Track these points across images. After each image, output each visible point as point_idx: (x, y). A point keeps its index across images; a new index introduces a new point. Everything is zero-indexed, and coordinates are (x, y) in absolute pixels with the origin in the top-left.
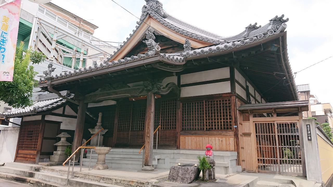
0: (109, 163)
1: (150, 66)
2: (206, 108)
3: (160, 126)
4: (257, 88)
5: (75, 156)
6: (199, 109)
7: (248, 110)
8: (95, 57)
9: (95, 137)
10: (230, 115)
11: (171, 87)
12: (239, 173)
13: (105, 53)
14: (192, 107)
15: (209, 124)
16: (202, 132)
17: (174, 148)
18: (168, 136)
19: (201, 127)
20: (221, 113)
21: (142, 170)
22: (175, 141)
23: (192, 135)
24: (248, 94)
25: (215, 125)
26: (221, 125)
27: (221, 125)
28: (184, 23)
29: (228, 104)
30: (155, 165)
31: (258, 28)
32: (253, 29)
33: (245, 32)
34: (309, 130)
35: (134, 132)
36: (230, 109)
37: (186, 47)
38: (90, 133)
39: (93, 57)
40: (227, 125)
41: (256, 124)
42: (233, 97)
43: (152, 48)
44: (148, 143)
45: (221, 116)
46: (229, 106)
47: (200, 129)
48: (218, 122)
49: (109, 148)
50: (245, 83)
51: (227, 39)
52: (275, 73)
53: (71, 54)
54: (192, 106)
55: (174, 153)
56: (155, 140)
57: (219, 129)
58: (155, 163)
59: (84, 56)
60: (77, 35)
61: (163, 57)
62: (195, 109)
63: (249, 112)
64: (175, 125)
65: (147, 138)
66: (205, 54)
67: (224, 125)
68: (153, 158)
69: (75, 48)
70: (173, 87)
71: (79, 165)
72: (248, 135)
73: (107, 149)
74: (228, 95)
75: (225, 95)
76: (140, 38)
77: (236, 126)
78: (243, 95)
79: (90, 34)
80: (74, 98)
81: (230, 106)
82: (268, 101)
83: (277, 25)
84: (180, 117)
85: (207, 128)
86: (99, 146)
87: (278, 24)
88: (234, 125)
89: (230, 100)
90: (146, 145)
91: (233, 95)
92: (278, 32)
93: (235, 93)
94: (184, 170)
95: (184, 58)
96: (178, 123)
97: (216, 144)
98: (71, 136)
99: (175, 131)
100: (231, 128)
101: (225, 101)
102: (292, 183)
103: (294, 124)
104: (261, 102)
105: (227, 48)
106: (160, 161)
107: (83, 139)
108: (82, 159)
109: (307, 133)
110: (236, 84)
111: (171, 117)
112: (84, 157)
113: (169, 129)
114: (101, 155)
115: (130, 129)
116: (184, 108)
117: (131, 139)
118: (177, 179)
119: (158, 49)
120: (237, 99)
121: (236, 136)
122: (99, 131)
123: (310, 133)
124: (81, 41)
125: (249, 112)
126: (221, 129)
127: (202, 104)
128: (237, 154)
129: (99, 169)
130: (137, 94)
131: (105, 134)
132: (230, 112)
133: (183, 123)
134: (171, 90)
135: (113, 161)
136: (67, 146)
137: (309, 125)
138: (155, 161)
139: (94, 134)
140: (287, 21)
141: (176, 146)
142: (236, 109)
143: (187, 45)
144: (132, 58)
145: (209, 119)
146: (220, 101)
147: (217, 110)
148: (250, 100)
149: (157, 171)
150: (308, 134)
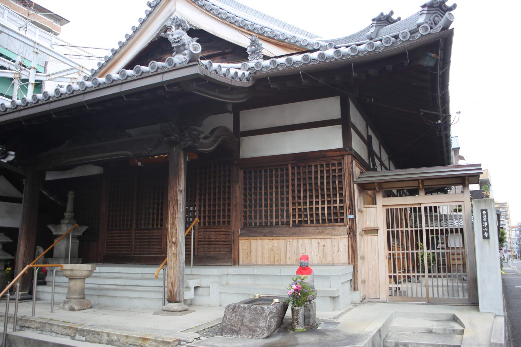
0: (94, 295)
1: (176, 88)
2: (293, 180)
3: (197, 219)
4: (383, 143)
5: (18, 284)
6: (279, 183)
7: (374, 183)
8: (60, 77)
9: (61, 241)
10: (341, 195)
11: (219, 137)
12: (356, 306)
13: (81, 69)
14: (263, 179)
15: (300, 213)
16: (284, 229)
17: (227, 262)
18: (213, 239)
19: (284, 218)
20: (323, 190)
21: (164, 311)
22: (229, 250)
23: (265, 236)
24: (371, 153)
25: (312, 215)
26: (323, 214)
27: (323, 214)
28: (245, 7)
29: (337, 171)
30: (190, 300)
31: (395, 21)
32: (386, 23)
33: (371, 27)
34: (485, 220)
35: (142, 231)
36: (340, 182)
37: (253, 52)
38: (52, 233)
39: (56, 78)
40: (336, 214)
41: (387, 210)
42: (346, 158)
43: (181, 48)
44: (172, 256)
45: (323, 196)
46: (340, 176)
47: (280, 223)
48: (317, 209)
49: (92, 266)
50: (365, 129)
51: (333, 41)
52: (422, 112)
53: (10, 71)
54: (263, 176)
55: (227, 274)
56: (188, 253)
57: (319, 223)
58: (189, 295)
59: (38, 75)
60: (22, 32)
61: (206, 68)
62: (271, 182)
63: (377, 188)
64: (229, 216)
65: (170, 247)
66: (295, 66)
67: (329, 214)
68: (185, 286)
69: (18, 59)
70: (225, 137)
71: (31, 299)
72: (374, 231)
73: (87, 267)
74: (338, 153)
75: (332, 154)
76: (153, 35)
77: (352, 216)
78: (363, 154)
79: (52, 34)
80: (16, 161)
81: (341, 175)
82: (398, 166)
83: (435, 15)
84: (239, 201)
85: (294, 222)
86: (71, 263)
87: (437, 14)
88: (348, 213)
89: (341, 163)
90: (170, 259)
91: (347, 153)
92: (437, 29)
93: (351, 149)
94: (255, 313)
95: (250, 73)
96: (234, 212)
97: (313, 253)
98: (11, 241)
99: (228, 230)
100: (342, 220)
101: (330, 165)
102: (455, 319)
103: (435, 208)
104: (388, 168)
105: (340, 56)
106: (200, 290)
107: (38, 247)
108: (37, 288)
109: (483, 225)
110: (353, 133)
111: (219, 199)
112: (39, 284)
113: (217, 224)
114: (75, 280)
115: (134, 226)
116: (248, 180)
117: (135, 245)
118: (240, 330)
119: (195, 49)
120: (354, 162)
121: (352, 234)
122: (69, 229)
123: (488, 226)
124: (32, 44)
125: (377, 188)
126: (322, 223)
127: (285, 172)
128: (353, 270)
129: (72, 309)
130: (146, 151)
131: (81, 235)
132: (341, 189)
133: (245, 212)
134: (221, 143)
135: (100, 293)
136: (6, 261)
137: (486, 210)
138: (190, 290)
139: (60, 236)
140: (453, 8)
141: (231, 258)
142: (354, 181)
143: (254, 47)
144: (137, 72)
145: (299, 204)
146: (322, 166)
147: (316, 184)
148: (374, 164)
149: (194, 311)
150: (483, 227)
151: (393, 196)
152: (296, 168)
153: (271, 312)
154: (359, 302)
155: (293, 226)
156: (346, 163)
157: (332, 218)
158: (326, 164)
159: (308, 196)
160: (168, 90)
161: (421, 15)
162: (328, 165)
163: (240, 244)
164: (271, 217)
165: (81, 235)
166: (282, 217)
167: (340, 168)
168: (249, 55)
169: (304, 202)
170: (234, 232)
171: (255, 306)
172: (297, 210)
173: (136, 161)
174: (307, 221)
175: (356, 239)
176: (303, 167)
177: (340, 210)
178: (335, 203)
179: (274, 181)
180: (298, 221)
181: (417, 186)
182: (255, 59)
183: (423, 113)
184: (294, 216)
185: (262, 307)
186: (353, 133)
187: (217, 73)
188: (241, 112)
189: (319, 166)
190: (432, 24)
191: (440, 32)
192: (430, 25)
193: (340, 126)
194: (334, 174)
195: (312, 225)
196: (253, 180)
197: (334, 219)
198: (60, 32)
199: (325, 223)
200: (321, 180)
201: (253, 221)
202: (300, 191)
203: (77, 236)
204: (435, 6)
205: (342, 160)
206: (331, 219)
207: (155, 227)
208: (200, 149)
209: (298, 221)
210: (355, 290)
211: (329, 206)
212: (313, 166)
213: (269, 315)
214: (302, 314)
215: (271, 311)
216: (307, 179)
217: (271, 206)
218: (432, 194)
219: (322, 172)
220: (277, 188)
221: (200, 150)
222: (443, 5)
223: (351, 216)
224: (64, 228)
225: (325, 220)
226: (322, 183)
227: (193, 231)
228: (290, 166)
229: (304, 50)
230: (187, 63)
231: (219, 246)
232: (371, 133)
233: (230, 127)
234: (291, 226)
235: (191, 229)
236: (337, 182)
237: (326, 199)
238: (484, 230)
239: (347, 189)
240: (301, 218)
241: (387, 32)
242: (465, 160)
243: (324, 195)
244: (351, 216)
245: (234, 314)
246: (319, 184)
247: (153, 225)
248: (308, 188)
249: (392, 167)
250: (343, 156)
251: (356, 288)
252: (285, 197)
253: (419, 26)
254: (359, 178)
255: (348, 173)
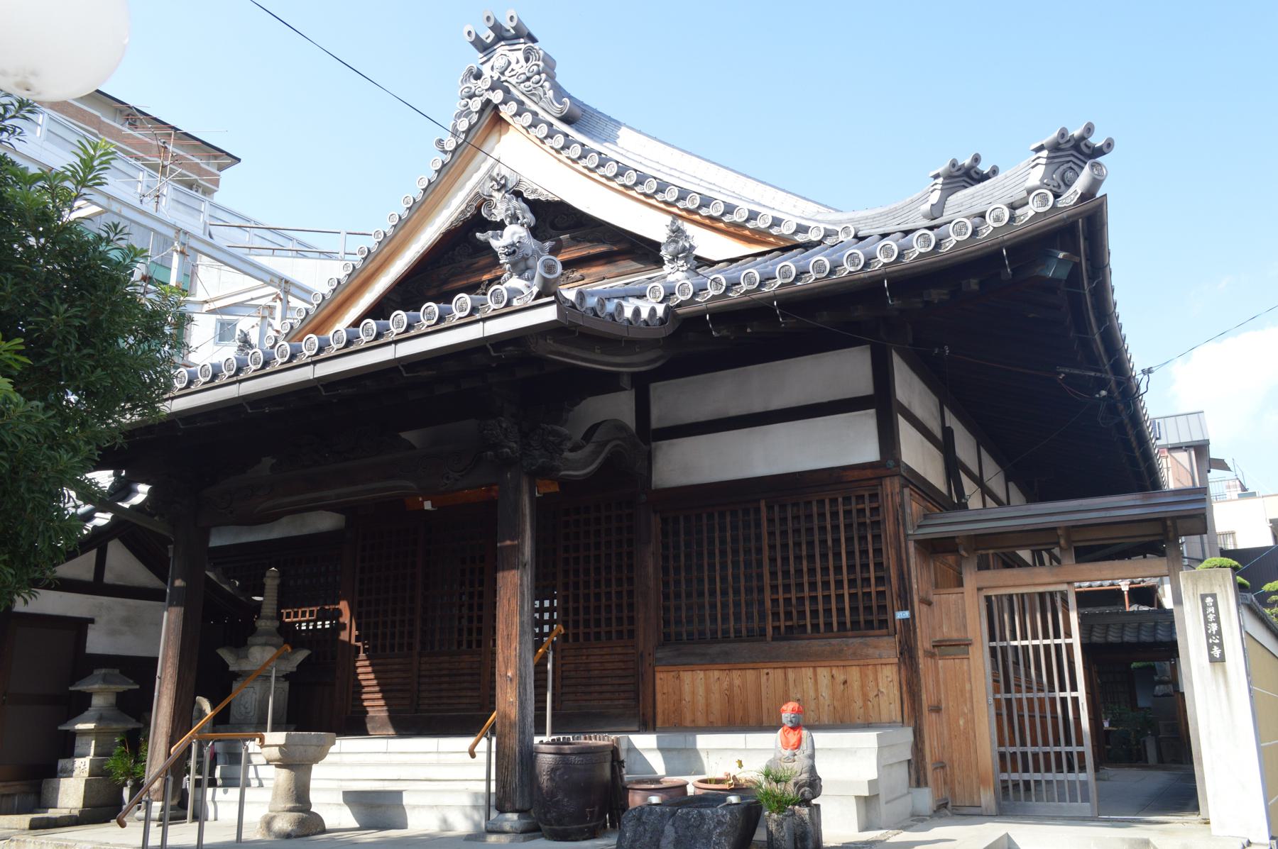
2: (771, 534)
4: (987, 439)
10: (879, 565)
15: (789, 608)
20: (837, 555)
24: (953, 467)
25: (815, 613)
26: (841, 611)
27: (841, 611)
34: (1211, 617)
36: (877, 538)
40: (868, 609)
45: (838, 569)
46: (877, 524)
47: (744, 632)
50: (937, 414)
54: (705, 529)
62: (723, 542)
67: (854, 610)
74: (869, 473)
80: (148, 504)
83: (1066, 166)
88: (896, 608)
92: (1070, 197)
93: (898, 461)
97: (821, 698)
100: (883, 624)
101: (853, 500)
104: (1005, 500)
109: (1207, 630)
110: (903, 424)
121: (908, 655)
123: (1219, 632)
126: (839, 630)
131: (295, 670)
132: (878, 551)
137: (1214, 596)
145: (787, 588)
146: (834, 501)
150: (1208, 636)
151: (1019, 566)
152: (776, 508)
153: (720, 823)
154: (929, 814)
155: (774, 639)
156: (887, 495)
157: (862, 618)
158: (844, 499)
159: (805, 569)
160: (495, 354)
161: (1033, 167)
162: (847, 500)
163: (658, 682)
164: (725, 619)
165: (295, 670)
166: (750, 617)
167: (875, 505)
168: (666, 262)
169: (796, 585)
170: (641, 655)
171: (685, 810)
172: (781, 601)
173: (420, 499)
174: (805, 626)
175: (917, 664)
176: (794, 505)
177: (877, 600)
178: (865, 585)
179: (729, 539)
180: (786, 627)
181: (1162, 534)
182: (678, 270)
183: (1063, 375)
184: (776, 615)
185: (699, 812)
186: (903, 424)
187: (596, 314)
188: (653, 386)
189: (827, 502)
190: (1059, 186)
191: (1075, 204)
192: (1055, 189)
193: (872, 411)
194: (862, 520)
195: (817, 635)
196: (683, 536)
197: (866, 622)
198: (218, 186)
199: (845, 630)
200: (832, 533)
201: (684, 630)
202: (788, 559)
203: (285, 673)
204: (1063, 146)
205: (879, 487)
206: (859, 622)
207: (464, 647)
208: (563, 473)
209: (786, 627)
210: (918, 785)
211: (853, 591)
212: (814, 503)
213: (715, 828)
214: (788, 828)
215: (721, 820)
216: (803, 531)
217: (724, 593)
218: (1145, 557)
219: (835, 515)
220: (735, 552)
221: (563, 475)
222: (1084, 142)
223: (902, 615)
224: (260, 655)
225: (845, 623)
226: (837, 541)
227: (551, 653)
228: (763, 504)
229: (788, 244)
230: (533, 297)
231: (609, 688)
232: (952, 421)
233: (629, 419)
234: (769, 638)
235: (548, 649)
236: (869, 538)
237: (780, 581)
238: (1211, 641)
239: (892, 553)
240: (791, 619)
241: (967, 200)
242: (1228, 469)
243: (841, 568)
244: (902, 615)
245: (641, 829)
246: (830, 543)
247: (460, 644)
248: (804, 553)
249: (1016, 496)
250: (880, 478)
251: (922, 779)
252: (754, 574)
253: (1030, 192)
254: (920, 527)
255: (894, 517)
